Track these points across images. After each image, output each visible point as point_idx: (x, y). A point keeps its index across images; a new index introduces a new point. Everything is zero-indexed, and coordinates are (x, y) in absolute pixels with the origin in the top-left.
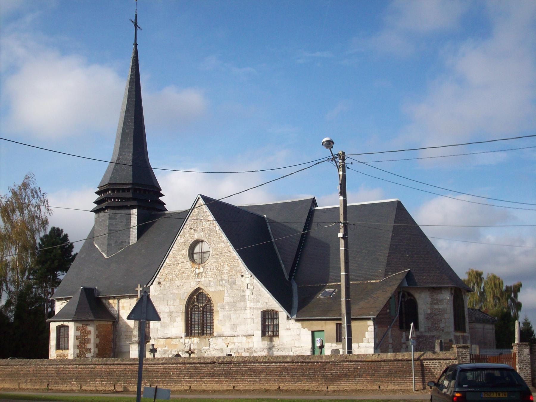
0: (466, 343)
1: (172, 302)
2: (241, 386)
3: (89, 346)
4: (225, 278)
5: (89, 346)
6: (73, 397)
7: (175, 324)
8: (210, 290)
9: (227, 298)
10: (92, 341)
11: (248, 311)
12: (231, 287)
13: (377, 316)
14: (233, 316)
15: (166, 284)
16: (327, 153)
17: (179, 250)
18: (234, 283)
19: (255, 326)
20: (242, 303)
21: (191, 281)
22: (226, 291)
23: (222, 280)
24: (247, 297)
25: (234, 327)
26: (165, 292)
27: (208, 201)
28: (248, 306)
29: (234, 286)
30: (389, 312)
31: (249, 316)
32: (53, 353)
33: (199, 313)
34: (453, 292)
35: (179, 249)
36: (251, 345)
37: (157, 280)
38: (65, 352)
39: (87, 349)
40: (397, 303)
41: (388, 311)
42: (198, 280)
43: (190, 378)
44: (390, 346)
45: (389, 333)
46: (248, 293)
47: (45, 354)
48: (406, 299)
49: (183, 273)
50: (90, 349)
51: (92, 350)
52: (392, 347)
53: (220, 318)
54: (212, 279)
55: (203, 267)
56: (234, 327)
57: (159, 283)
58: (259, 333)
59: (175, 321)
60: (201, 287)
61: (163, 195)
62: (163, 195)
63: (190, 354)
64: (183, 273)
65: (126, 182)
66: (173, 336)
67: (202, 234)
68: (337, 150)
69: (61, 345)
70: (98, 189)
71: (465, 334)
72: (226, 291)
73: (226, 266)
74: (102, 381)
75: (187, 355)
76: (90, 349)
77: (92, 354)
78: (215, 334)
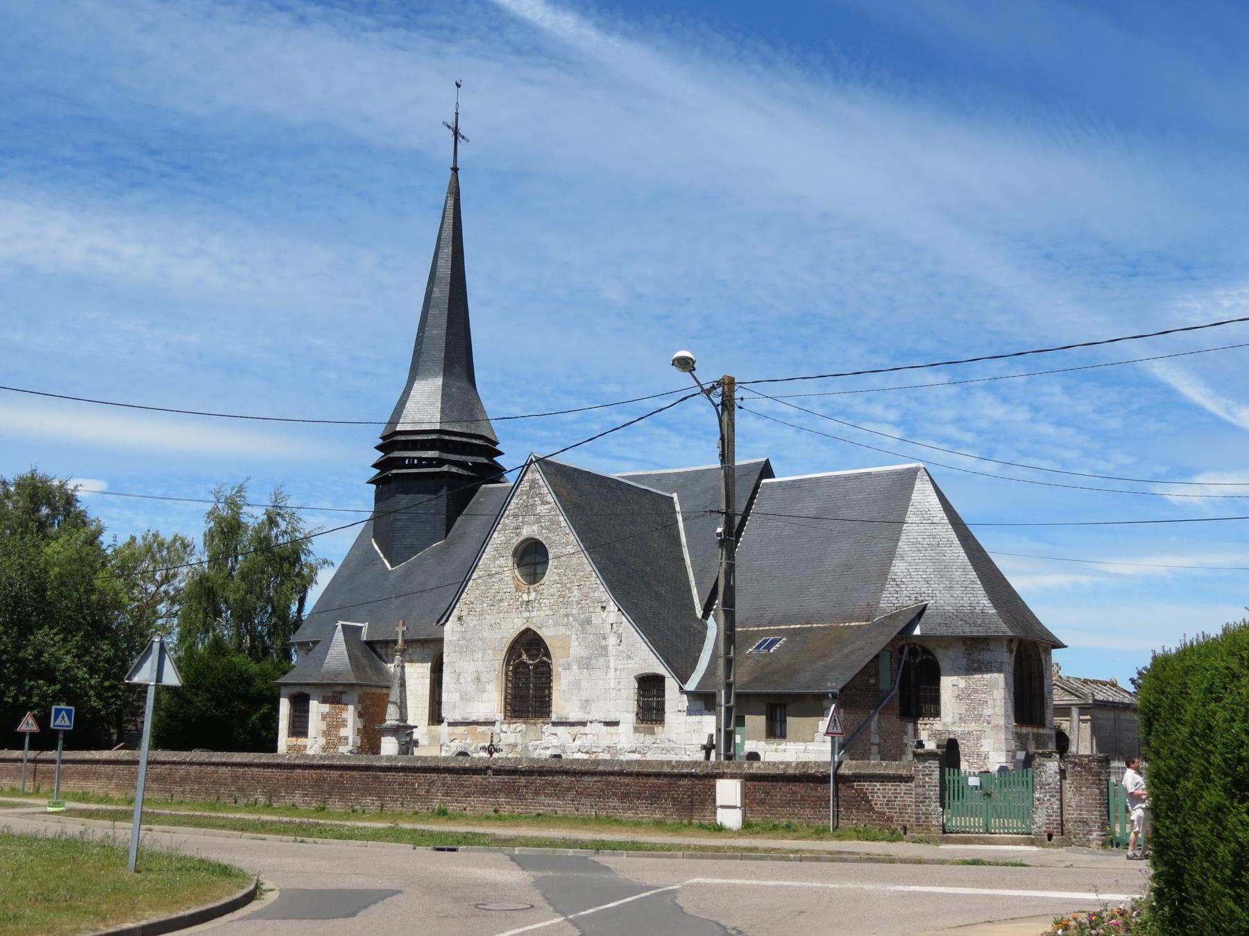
0: (1045, 746)
1: (480, 655)
2: (220, 815)
3: (343, 732)
4: (574, 611)
5: (343, 732)
6: (659, 825)
7: (485, 696)
8: (545, 633)
9: (577, 649)
10: (350, 723)
11: (612, 674)
12: (583, 629)
13: (841, 691)
14: (585, 684)
15: (471, 621)
16: (683, 380)
17: (495, 558)
18: (588, 621)
19: (625, 705)
20: (602, 660)
21: (513, 615)
22: (574, 637)
23: (567, 616)
24: (610, 648)
25: (586, 704)
26: (469, 636)
27: (545, 464)
28: (612, 665)
29: (588, 627)
30: (876, 684)
31: (613, 684)
32: (284, 741)
33: (529, 679)
34: (1014, 647)
35: (494, 556)
36: (615, 739)
37: (456, 612)
38: (301, 741)
39: (340, 738)
40: (895, 666)
41: (872, 681)
42: (526, 614)
43: (447, 794)
44: (875, 749)
45: (874, 725)
46: (612, 640)
47: (272, 746)
48: (918, 660)
49: (501, 601)
50: (346, 738)
51: (350, 741)
52: (880, 752)
53: (563, 687)
54: (550, 613)
55: (535, 590)
56: (586, 704)
57: (460, 618)
58: (631, 717)
59: (484, 691)
60: (532, 627)
61: (501, 453)
62: (501, 453)
63: (491, 755)
64: (501, 601)
65: (427, 427)
66: (482, 720)
67: (535, 527)
68: (708, 374)
69: (299, 727)
70: (381, 441)
71: (1041, 731)
72: (574, 637)
73: (575, 589)
74: (306, 795)
75: (485, 755)
76: (346, 738)
77: (350, 747)
78: (554, 718)
